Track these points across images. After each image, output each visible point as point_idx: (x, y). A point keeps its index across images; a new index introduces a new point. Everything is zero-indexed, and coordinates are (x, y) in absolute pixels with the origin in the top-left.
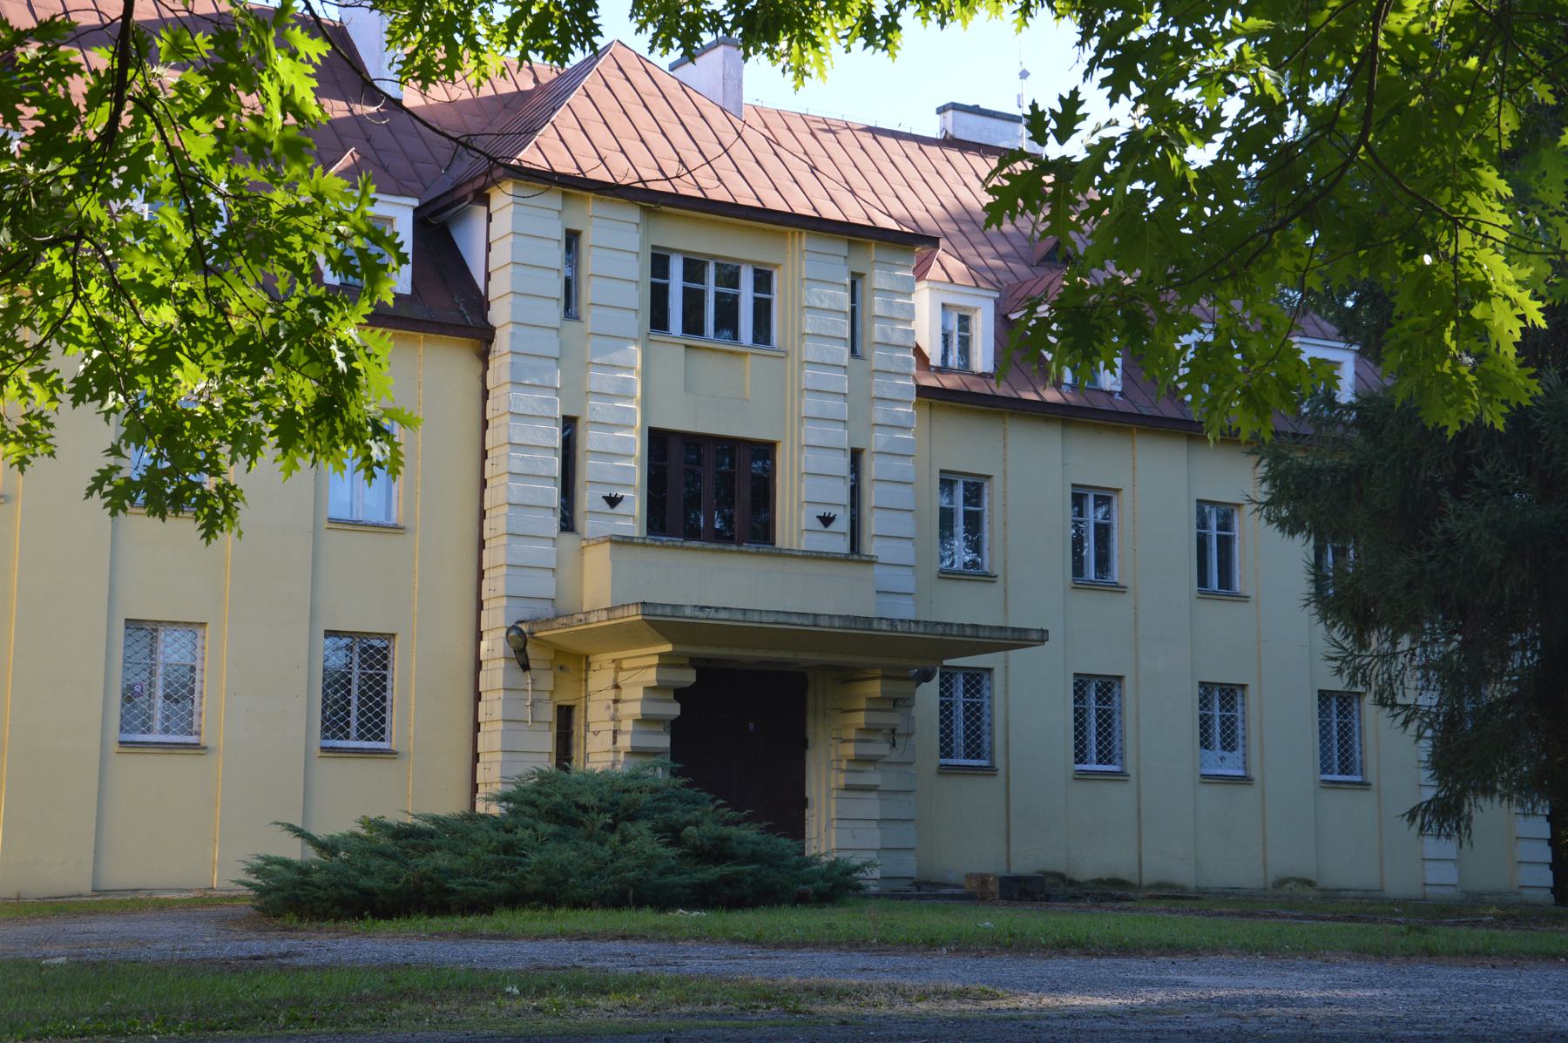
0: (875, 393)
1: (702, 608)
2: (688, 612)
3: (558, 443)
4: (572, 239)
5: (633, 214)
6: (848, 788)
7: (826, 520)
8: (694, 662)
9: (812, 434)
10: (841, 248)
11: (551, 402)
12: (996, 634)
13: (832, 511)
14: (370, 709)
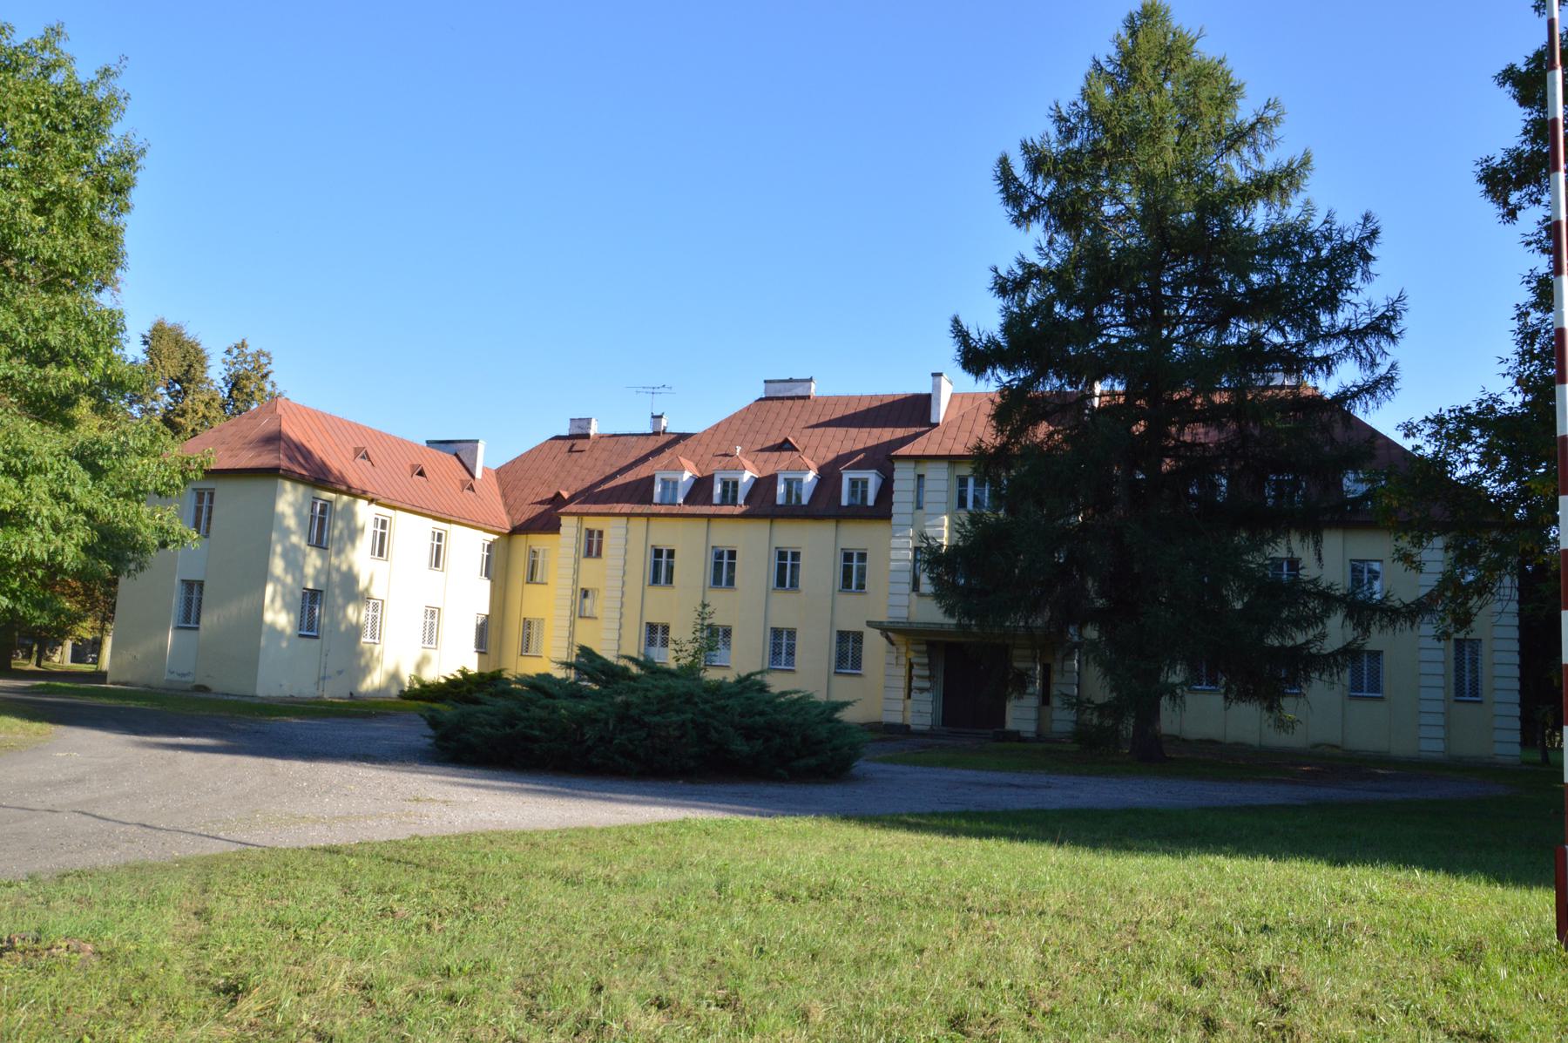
4: (921, 477)
5: (945, 465)
10: (912, 465)
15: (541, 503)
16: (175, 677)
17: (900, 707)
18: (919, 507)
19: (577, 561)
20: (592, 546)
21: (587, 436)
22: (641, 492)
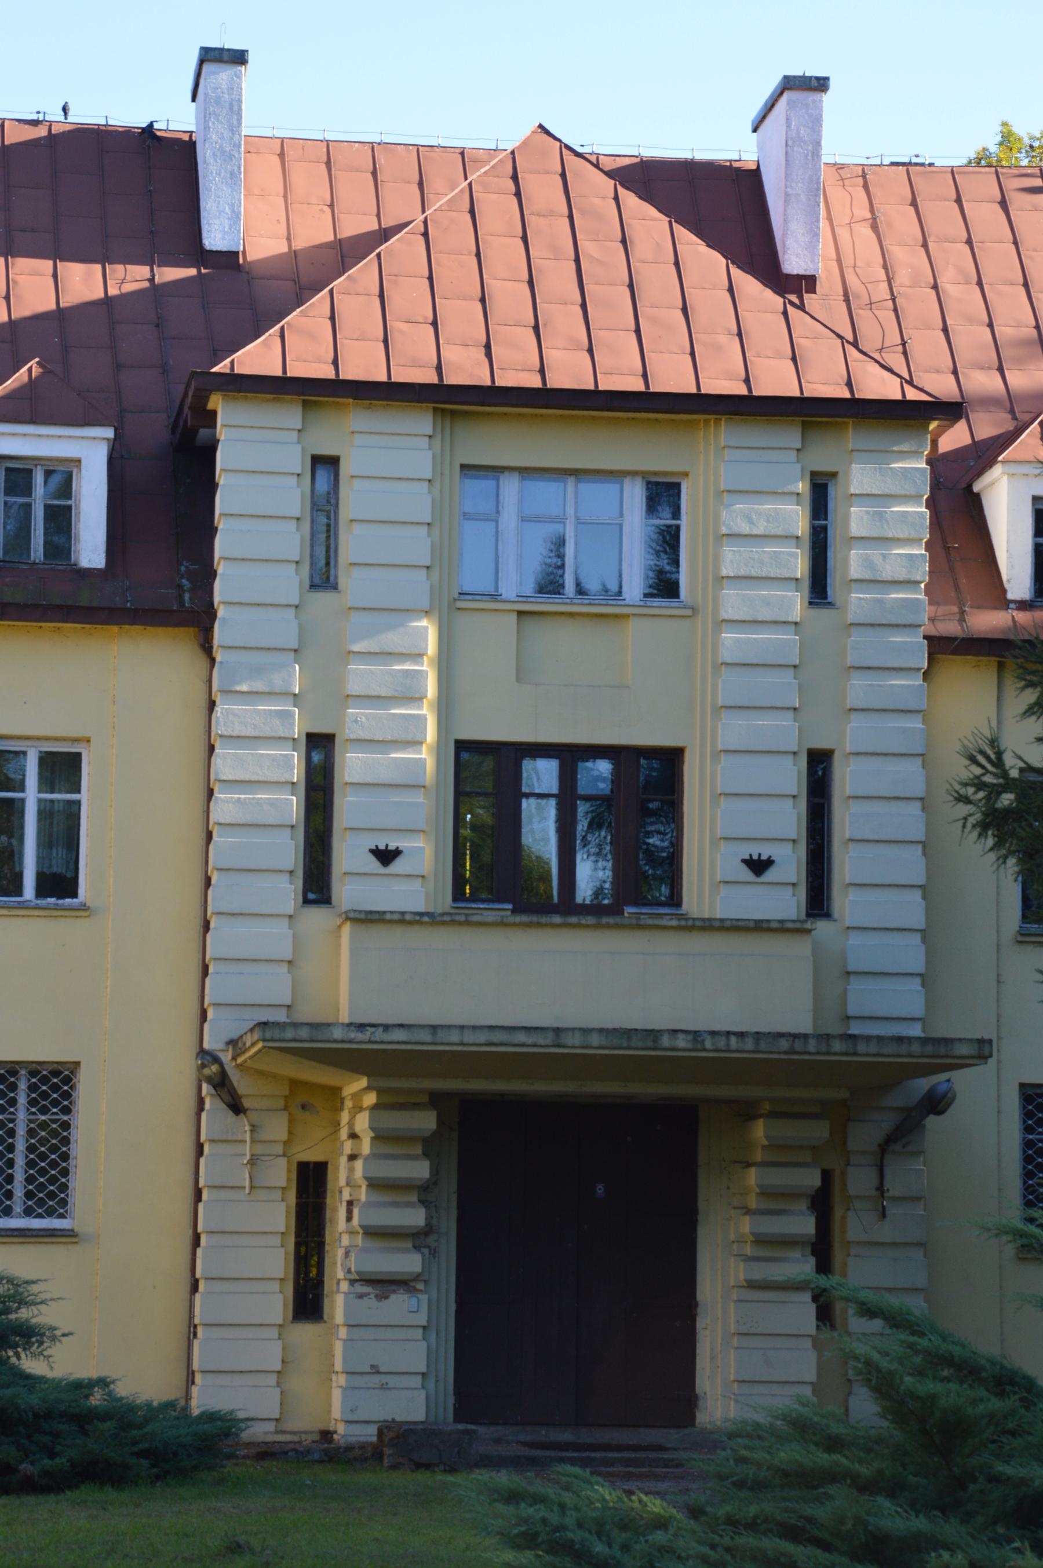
0: (850, 661)
1: (361, 1027)
2: (337, 1033)
3: (297, 773)
4: (325, 464)
5: (420, 422)
6: (752, 1285)
7: (758, 866)
8: (436, 1100)
9: (735, 730)
10: (790, 436)
11: (286, 715)
12: (889, 1049)
13: (765, 851)
14: (43, 1172)
15: (951, 568)
17: (271, 1357)
18: (323, 578)
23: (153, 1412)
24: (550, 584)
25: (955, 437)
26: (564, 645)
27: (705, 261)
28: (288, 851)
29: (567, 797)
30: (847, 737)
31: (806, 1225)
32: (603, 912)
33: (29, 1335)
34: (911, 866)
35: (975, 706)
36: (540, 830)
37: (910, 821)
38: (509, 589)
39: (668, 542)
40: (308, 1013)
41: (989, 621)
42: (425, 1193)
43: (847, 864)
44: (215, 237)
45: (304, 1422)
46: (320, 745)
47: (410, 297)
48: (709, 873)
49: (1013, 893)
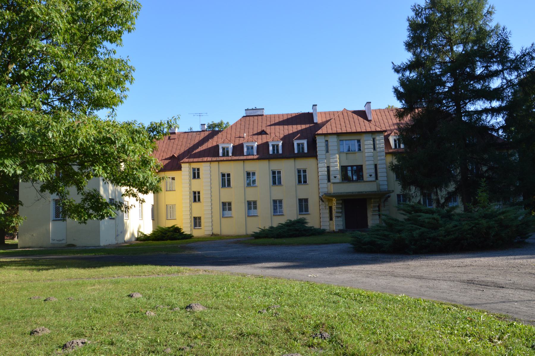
4: (327, 141)
5: (335, 136)
7: (371, 175)
8: (342, 200)
9: (367, 163)
10: (323, 137)
15: (166, 159)
16: (55, 242)
17: (328, 224)
18: (327, 151)
19: (190, 181)
20: (196, 174)
21: (174, 133)
22: (213, 152)
23: (318, 229)
24: (349, 150)
25: (386, 134)
26: (351, 156)
27: (361, 119)
28: (326, 177)
29: (352, 170)
30: (378, 163)
31: (377, 209)
32: (356, 181)
33: (306, 223)
34: (385, 174)
35: (390, 159)
36: (350, 173)
37: (385, 170)
38: (345, 151)
39: (360, 146)
40: (329, 192)
41: (391, 151)
42: (341, 208)
43: (379, 175)
44: (315, 121)
45: (332, 230)
46: (328, 167)
47: (334, 125)
48: (366, 177)
49: (395, 176)
